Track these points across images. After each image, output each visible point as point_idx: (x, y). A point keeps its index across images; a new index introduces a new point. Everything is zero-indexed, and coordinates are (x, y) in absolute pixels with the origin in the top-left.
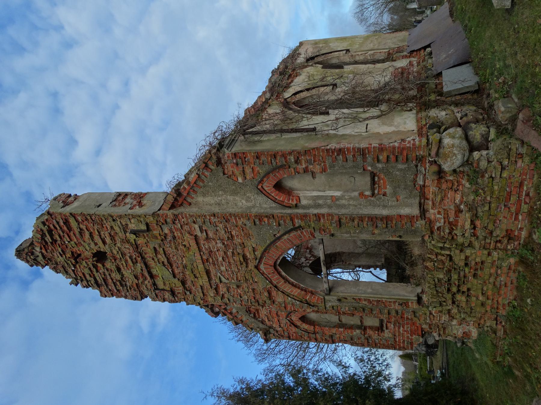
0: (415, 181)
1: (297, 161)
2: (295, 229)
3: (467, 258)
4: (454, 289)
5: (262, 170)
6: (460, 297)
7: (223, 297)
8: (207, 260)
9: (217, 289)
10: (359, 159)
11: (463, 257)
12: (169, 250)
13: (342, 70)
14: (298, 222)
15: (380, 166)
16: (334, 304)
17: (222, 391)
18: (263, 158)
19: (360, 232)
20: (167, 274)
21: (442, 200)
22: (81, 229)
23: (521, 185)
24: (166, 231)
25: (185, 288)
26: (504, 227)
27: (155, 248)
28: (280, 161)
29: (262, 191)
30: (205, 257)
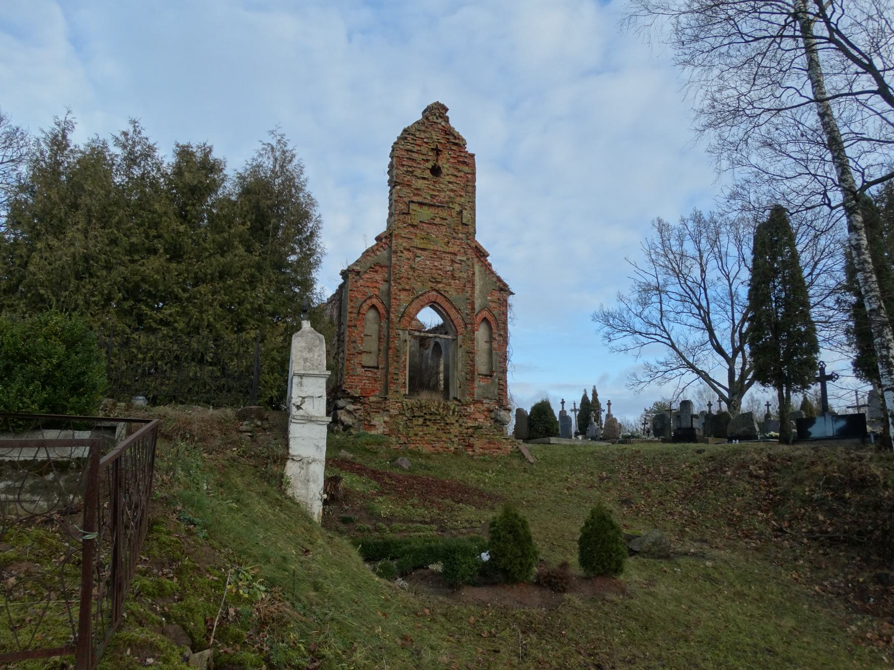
0: (488, 398)
1: (500, 335)
2: (466, 324)
3: (453, 424)
4: (428, 417)
5: (495, 312)
6: (421, 421)
7: (402, 252)
8: (435, 254)
9: (408, 250)
10: (501, 370)
11: (453, 422)
12: (443, 229)
13: (866, 415)
14: (469, 326)
15: (497, 380)
16: (401, 336)
17: (122, 138)
18: (503, 316)
19: (463, 364)
20: (425, 218)
21: (479, 412)
22: (459, 171)
23: (499, 449)
24: (460, 235)
25: (409, 225)
26: (476, 442)
27: (446, 219)
28: (502, 325)
29: (482, 309)
30: (438, 253)
